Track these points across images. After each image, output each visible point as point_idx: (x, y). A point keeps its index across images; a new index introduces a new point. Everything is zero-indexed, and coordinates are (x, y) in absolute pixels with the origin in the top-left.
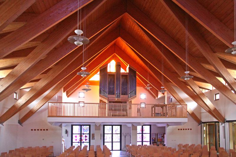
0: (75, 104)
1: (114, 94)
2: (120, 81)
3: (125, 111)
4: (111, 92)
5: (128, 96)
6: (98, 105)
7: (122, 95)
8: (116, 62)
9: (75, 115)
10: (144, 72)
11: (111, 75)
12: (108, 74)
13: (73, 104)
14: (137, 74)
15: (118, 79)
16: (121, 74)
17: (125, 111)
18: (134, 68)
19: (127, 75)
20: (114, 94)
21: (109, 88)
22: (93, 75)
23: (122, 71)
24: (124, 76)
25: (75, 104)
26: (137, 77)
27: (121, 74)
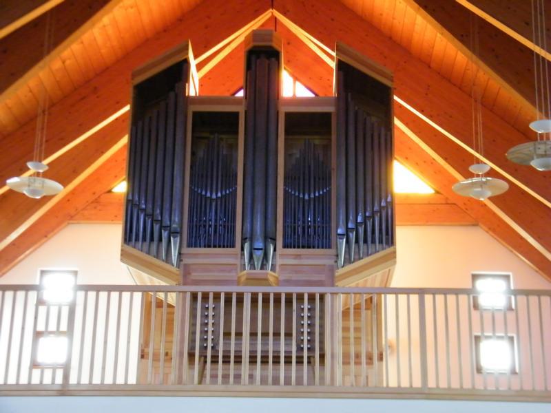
0: (428, 298)
1: (233, 246)
2: (270, 153)
3: (288, 335)
4: (210, 230)
5: (332, 251)
6: (138, 296)
7: (285, 246)
8: (257, 30)
9: (432, 383)
10: (450, 99)
11: (214, 123)
12: (193, 108)
13: (414, 298)
14: (395, 110)
15: (261, 147)
16: (283, 110)
17: (288, 335)
18: (374, 66)
19: (328, 115)
20: (233, 246)
21: (198, 206)
22: (463, 53)
23: (291, 88)
24: (304, 123)
25: (428, 298)
26: (397, 122)
27: (283, 110)
